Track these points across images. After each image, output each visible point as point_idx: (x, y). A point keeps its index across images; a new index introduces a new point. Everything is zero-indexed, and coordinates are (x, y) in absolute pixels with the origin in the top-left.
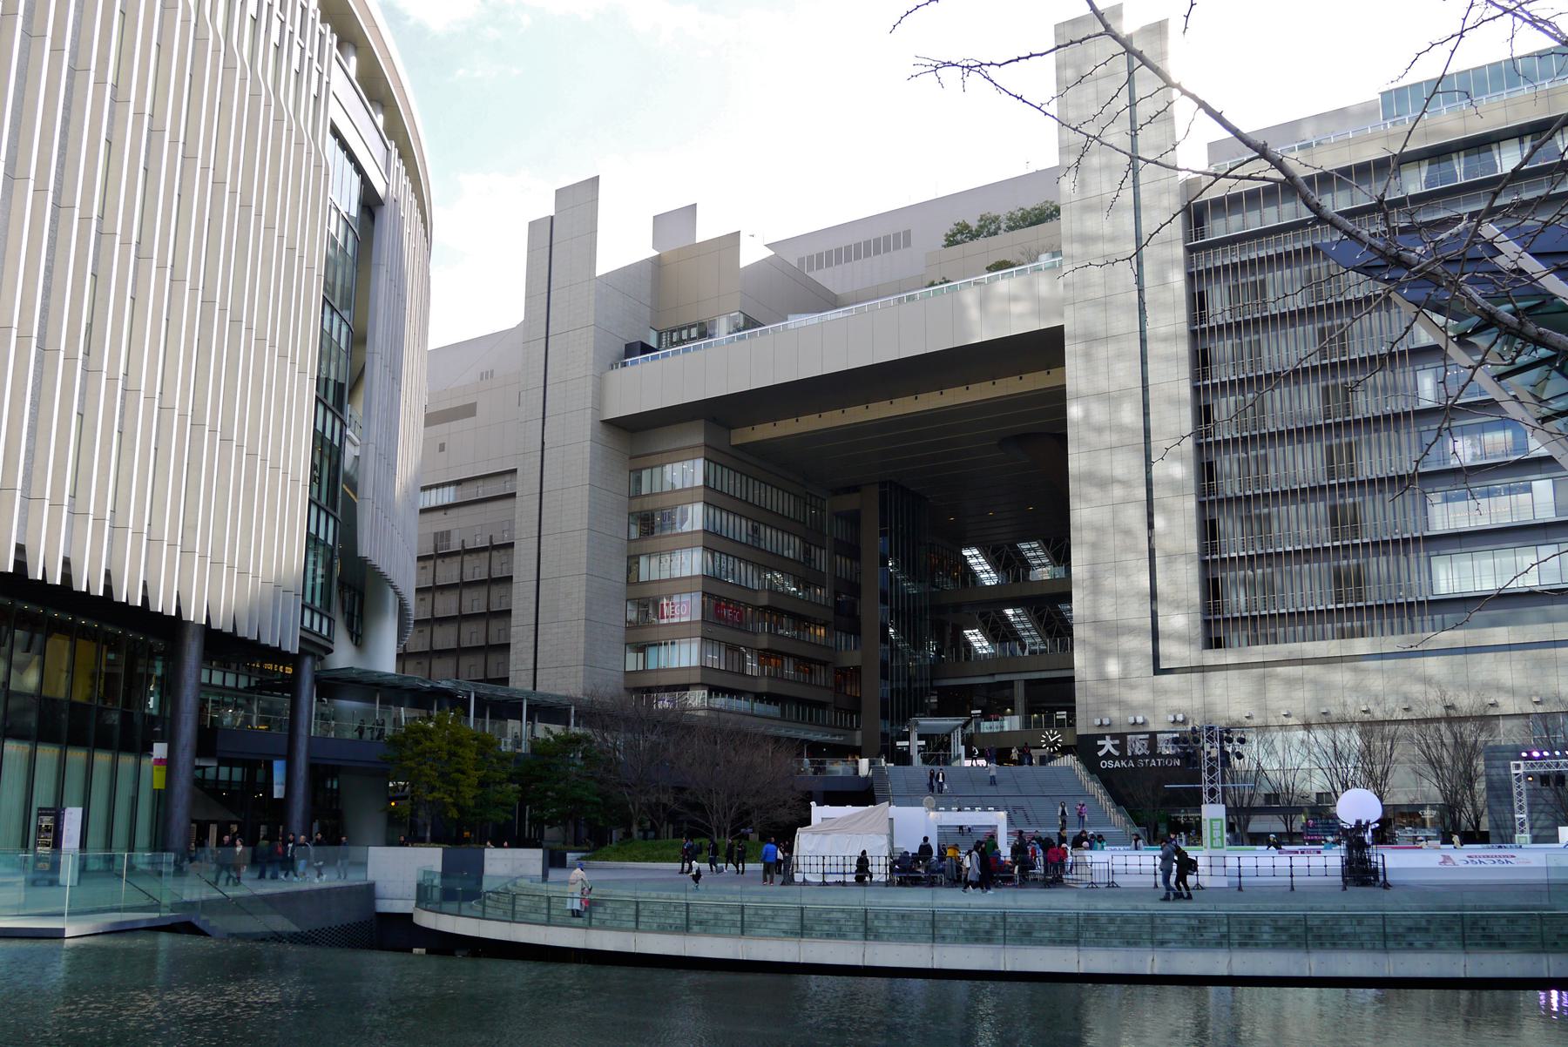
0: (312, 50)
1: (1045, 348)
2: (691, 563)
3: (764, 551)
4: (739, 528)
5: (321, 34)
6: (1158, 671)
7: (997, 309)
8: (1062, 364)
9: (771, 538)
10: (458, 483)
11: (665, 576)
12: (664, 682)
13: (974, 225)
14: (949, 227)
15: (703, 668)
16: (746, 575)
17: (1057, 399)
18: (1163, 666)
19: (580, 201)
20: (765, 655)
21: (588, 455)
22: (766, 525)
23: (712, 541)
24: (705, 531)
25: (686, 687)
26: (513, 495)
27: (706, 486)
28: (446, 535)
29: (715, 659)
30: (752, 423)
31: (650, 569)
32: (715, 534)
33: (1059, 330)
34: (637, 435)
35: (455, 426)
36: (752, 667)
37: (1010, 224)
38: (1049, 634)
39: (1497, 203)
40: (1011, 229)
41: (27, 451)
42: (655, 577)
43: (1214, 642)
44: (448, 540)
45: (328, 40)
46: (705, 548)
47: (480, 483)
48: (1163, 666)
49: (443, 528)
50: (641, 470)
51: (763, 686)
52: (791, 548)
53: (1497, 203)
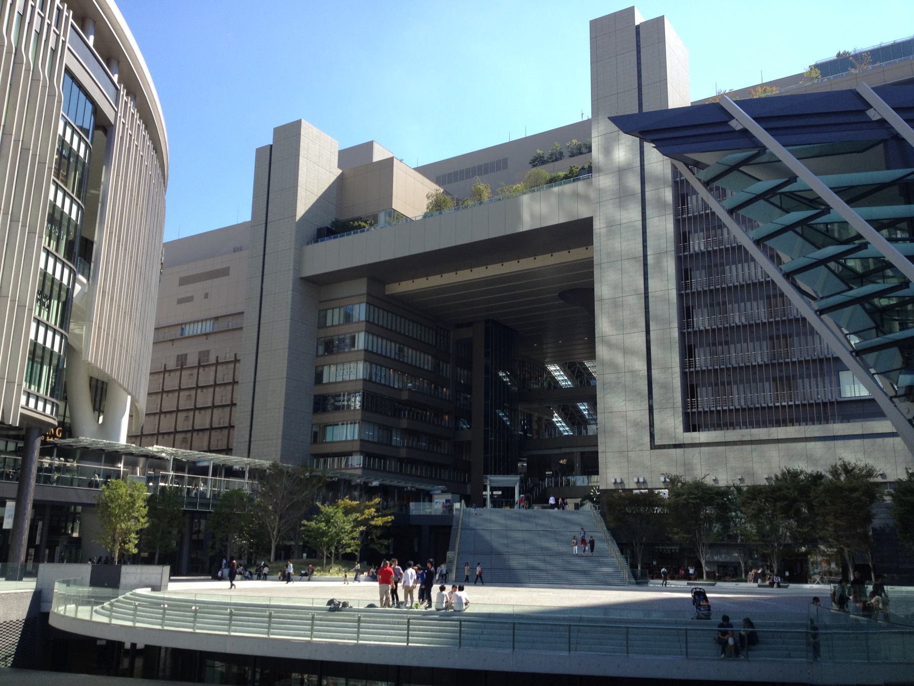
0: (50, 18)
1: (580, 232)
2: (357, 371)
3: (407, 364)
4: (390, 348)
5: (58, 8)
6: (653, 446)
7: (538, 210)
8: (592, 244)
9: (411, 355)
10: (216, 318)
11: (339, 379)
12: (336, 449)
13: (546, 156)
14: (531, 158)
15: (361, 440)
16: (394, 379)
17: (587, 268)
18: (658, 442)
19: (288, 137)
20: (407, 432)
21: (290, 300)
22: (409, 347)
23: (370, 356)
24: (366, 350)
25: (350, 454)
26: (241, 328)
27: (367, 321)
28: (206, 353)
29: (370, 434)
30: (399, 280)
31: (331, 374)
32: (372, 352)
33: (589, 222)
34: (317, 288)
35: (216, 281)
36: (396, 439)
37: (558, 157)
38: (573, 424)
39: (876, 376)
40: (571, 156)
41: (551, 250)
42: (333, 380)
43: (691, 425)
44: (208, 356)
45: (65, 13)
46: (365, 361)
47: (230, 318)
48: (658, 442)
49: (204, 348)
50: (327, 310)
51: (403, 453)
52: (426, 361)
53: (876, 376)
